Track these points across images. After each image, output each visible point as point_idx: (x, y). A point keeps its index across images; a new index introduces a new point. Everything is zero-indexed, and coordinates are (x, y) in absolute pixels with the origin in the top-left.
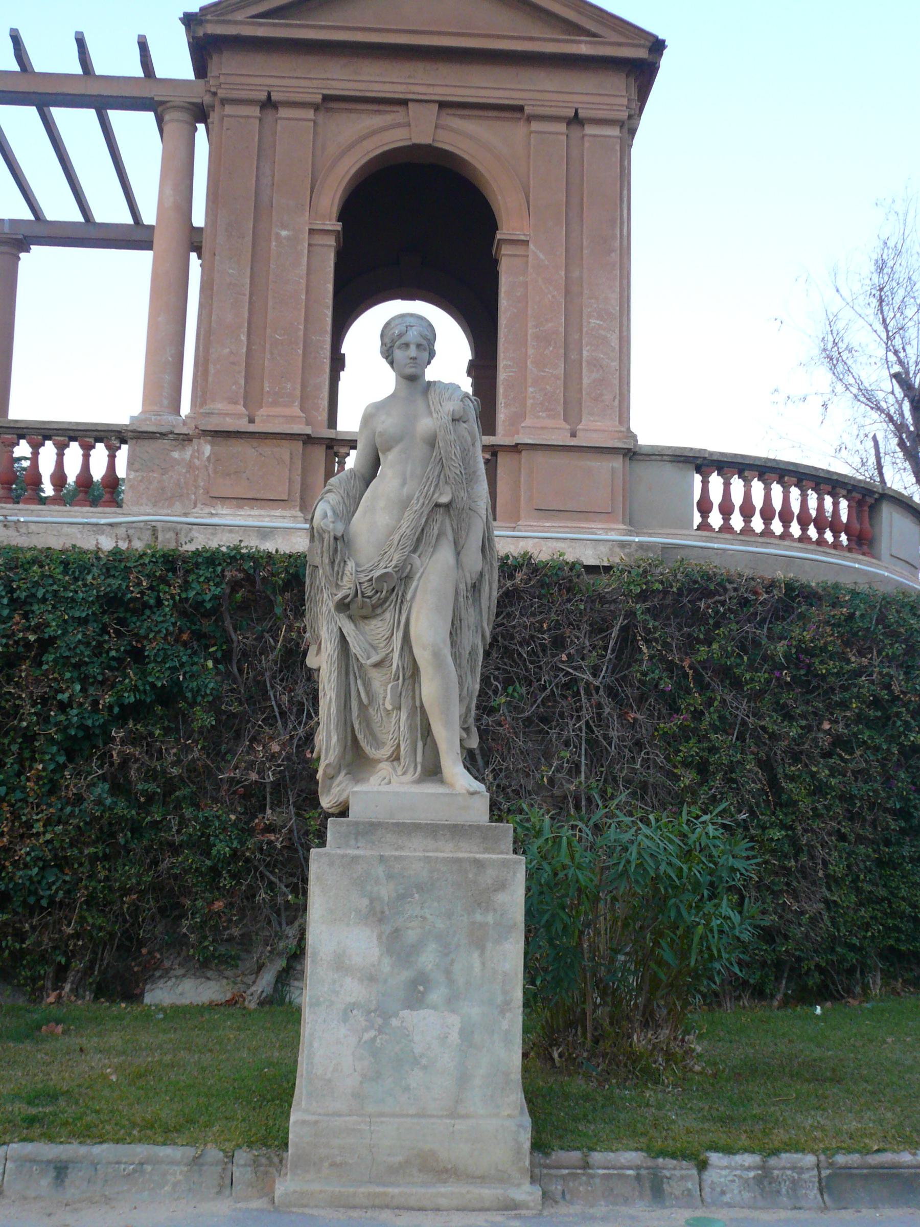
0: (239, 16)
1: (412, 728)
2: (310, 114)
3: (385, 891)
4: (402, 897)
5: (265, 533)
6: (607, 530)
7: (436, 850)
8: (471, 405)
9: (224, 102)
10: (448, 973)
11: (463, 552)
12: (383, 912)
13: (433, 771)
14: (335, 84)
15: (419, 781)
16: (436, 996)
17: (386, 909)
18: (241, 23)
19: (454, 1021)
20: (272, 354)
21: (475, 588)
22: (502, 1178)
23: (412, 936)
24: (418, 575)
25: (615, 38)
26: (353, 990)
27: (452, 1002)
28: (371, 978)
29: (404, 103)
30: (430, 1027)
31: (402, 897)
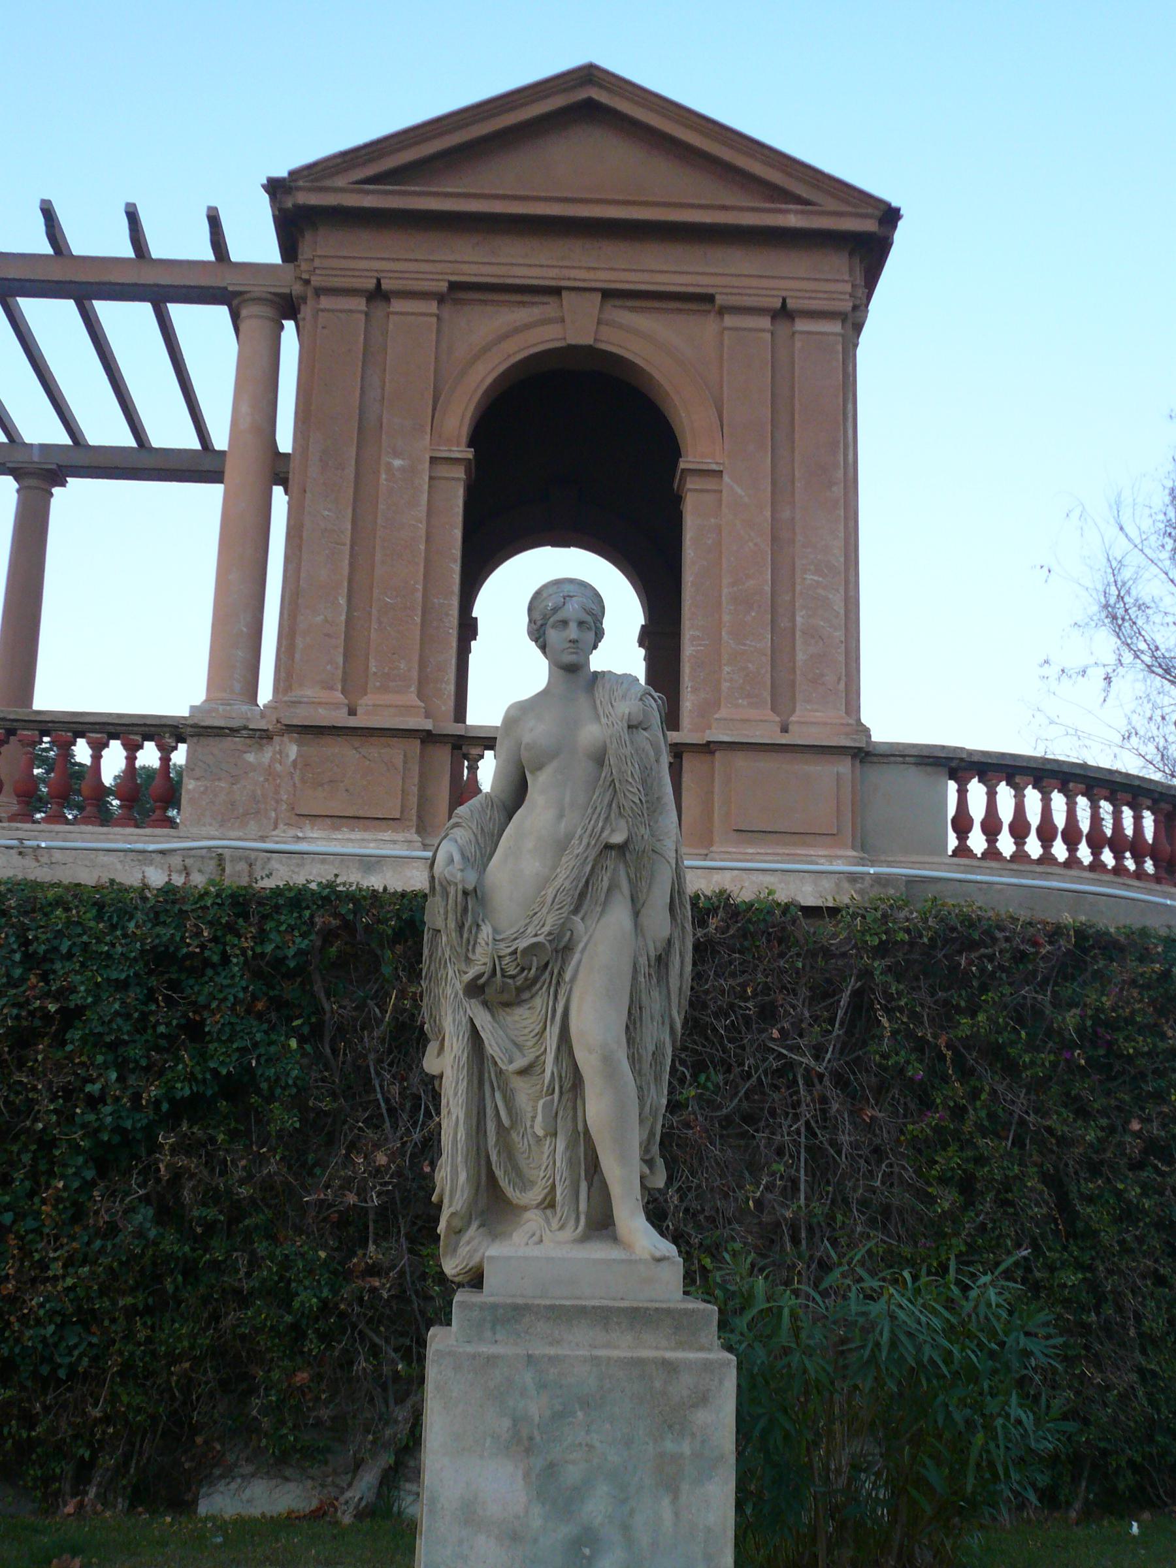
0: (340, 182)
2: (432, 307)
3: (535, 1408)
4: (560, 1416)
5: (369, 863)
6: (831, 858)
7: (607, 1346)
9: (319, 292)
10: (626, 1528)
12: (531, 1438)
14: (465, 268)
15: (584, 1238)
17: (536, 1432)
20: (380, 623)
21: (661, 961)
23: (573, 1474)
24: (581, 945)
25: (832, 205)
28: (513, 1536)
29: (556, 291)
31: (560, 1416)
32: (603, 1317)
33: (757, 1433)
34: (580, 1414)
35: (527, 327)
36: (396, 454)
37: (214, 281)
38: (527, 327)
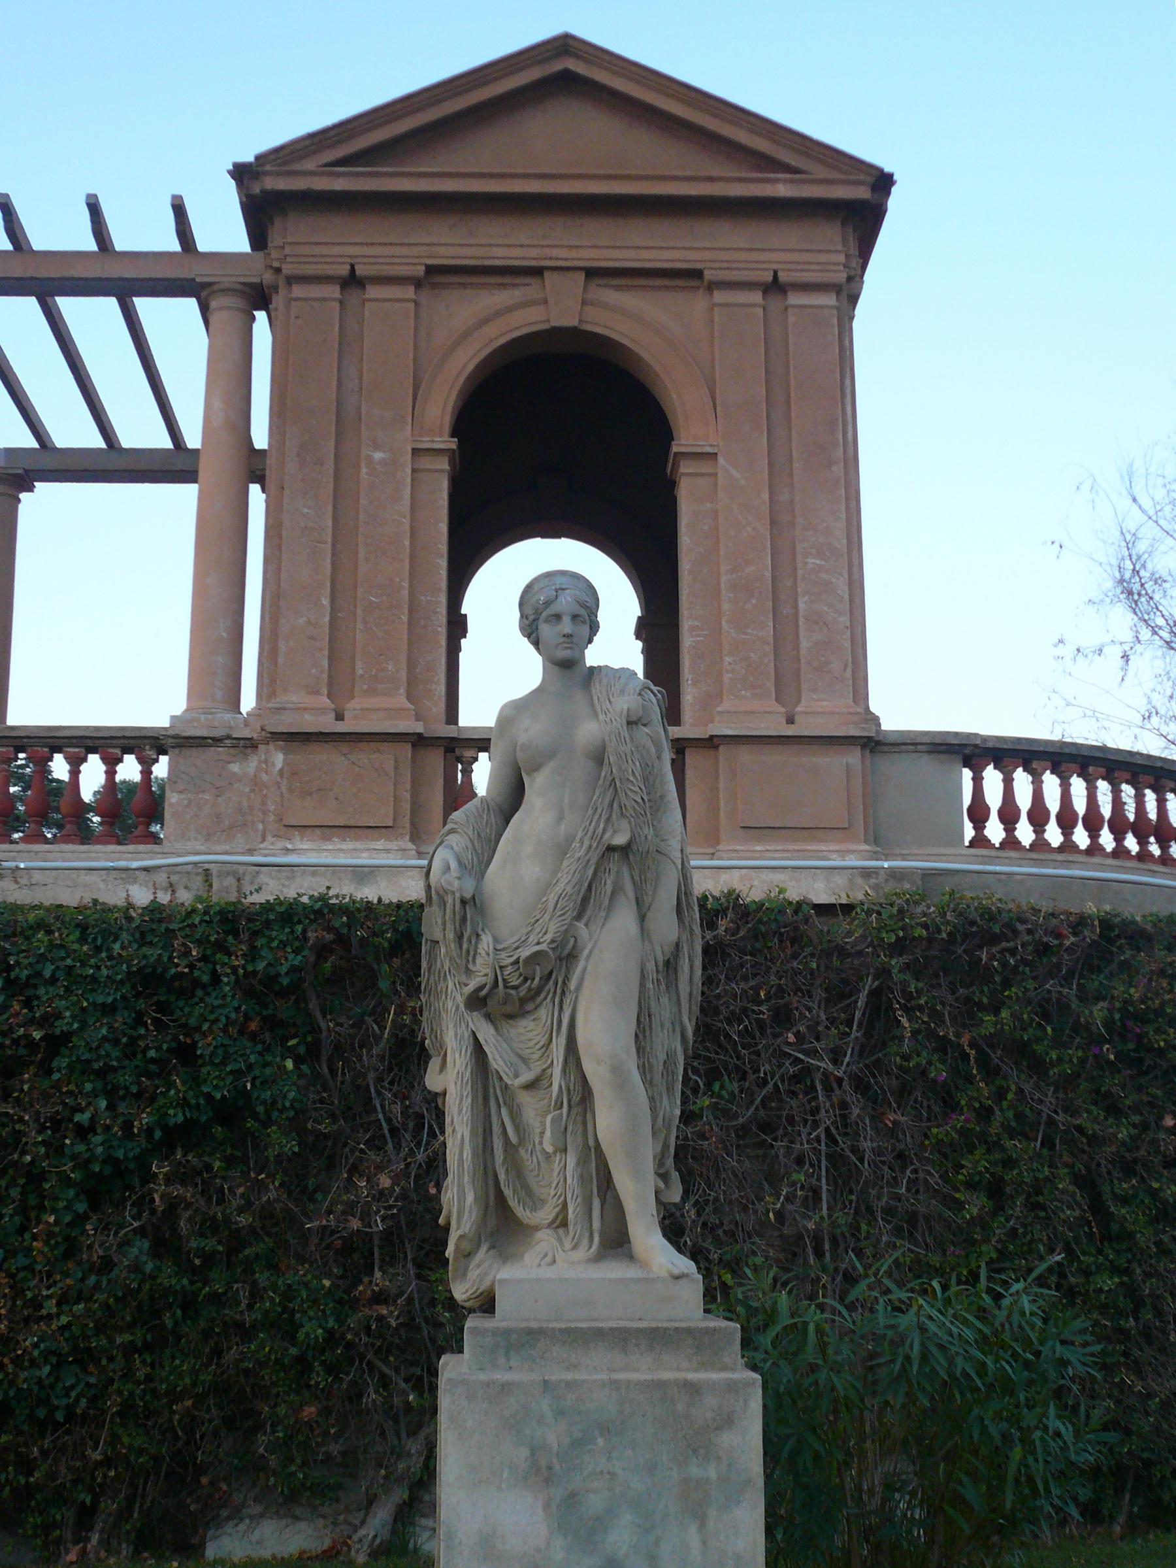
0: (309, 165)
2: (410, 292)
3: (554, 1436)
5: (362, 874)
6: (843, 853)
8: (654, 699)
9: (291, 280)
11: (649, 915)
12: (550, 1468)
15: (599, 1258)
18: (312, 173)
20: (365, 623)
21: (670, 966)
23: (595, 1503)
24: (586, 952)
25: (822, 172)
29: (537, 272)
31: (579, 1444)
32: (621, 1338)
34: (600, 1441)
36: (377, 446)
37: (182, 273)
38: (509, 309)
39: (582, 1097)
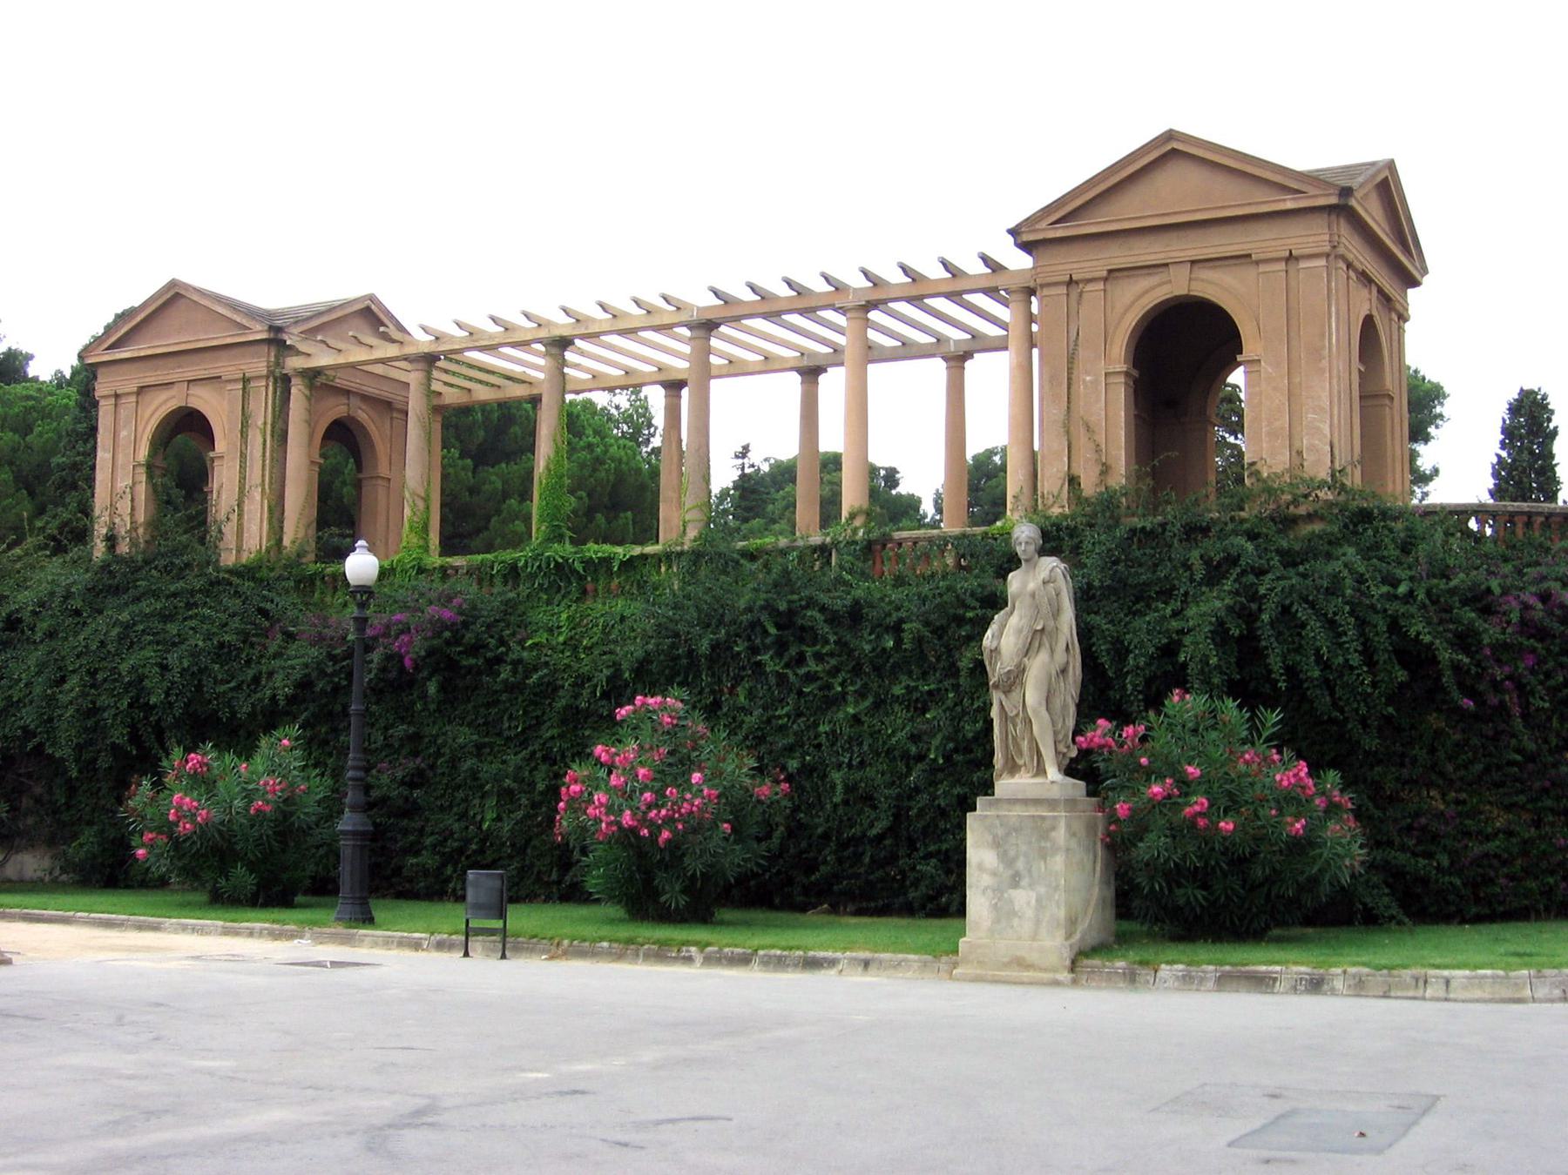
0: (1043, 225)
1: (1030, 749)
2: (1101, 286)
3: (1000, 832)
4: (1008, 834)
9: (1042, 286)
10: (1030, 871)
13: (1040, 771)
14: (1116, 261)
15: (1035, 776)
16: (1024, 882)
19: (1033, 895)
21: (1064, 671)
22: (1055, 970)
23: (1012, 853)
25: (1312, 191)
26: (986, 880)
27: (1031, 886)
28: (994, 874)
29: (1166, 265)
30: (1023, 898)
31: (1008, 834)
32: (1026, 802)
33: (232, 684)
35: (1153, 288)
37: (995, 280)
38: (1153, 288)
39: (1028, 722)
